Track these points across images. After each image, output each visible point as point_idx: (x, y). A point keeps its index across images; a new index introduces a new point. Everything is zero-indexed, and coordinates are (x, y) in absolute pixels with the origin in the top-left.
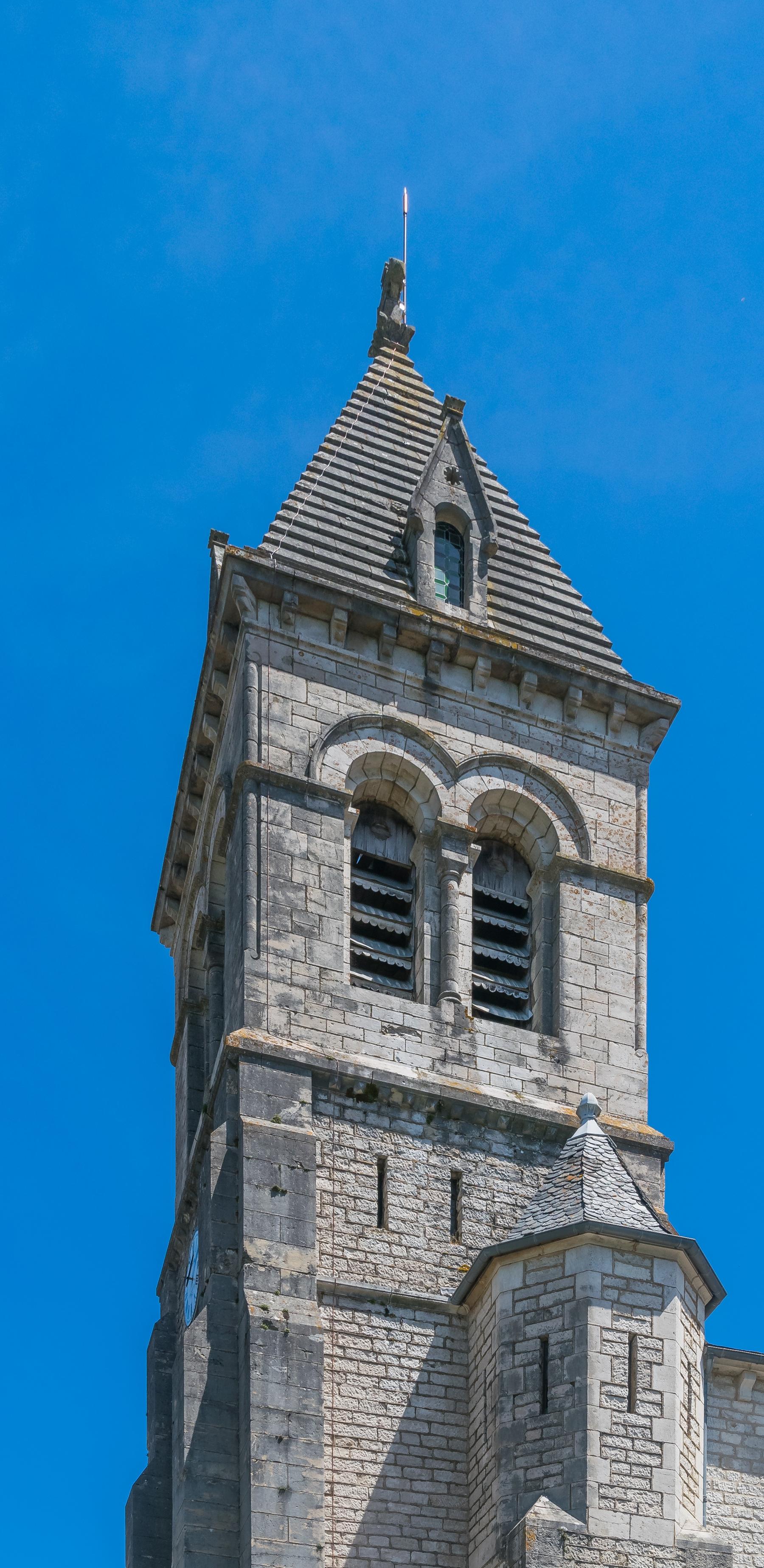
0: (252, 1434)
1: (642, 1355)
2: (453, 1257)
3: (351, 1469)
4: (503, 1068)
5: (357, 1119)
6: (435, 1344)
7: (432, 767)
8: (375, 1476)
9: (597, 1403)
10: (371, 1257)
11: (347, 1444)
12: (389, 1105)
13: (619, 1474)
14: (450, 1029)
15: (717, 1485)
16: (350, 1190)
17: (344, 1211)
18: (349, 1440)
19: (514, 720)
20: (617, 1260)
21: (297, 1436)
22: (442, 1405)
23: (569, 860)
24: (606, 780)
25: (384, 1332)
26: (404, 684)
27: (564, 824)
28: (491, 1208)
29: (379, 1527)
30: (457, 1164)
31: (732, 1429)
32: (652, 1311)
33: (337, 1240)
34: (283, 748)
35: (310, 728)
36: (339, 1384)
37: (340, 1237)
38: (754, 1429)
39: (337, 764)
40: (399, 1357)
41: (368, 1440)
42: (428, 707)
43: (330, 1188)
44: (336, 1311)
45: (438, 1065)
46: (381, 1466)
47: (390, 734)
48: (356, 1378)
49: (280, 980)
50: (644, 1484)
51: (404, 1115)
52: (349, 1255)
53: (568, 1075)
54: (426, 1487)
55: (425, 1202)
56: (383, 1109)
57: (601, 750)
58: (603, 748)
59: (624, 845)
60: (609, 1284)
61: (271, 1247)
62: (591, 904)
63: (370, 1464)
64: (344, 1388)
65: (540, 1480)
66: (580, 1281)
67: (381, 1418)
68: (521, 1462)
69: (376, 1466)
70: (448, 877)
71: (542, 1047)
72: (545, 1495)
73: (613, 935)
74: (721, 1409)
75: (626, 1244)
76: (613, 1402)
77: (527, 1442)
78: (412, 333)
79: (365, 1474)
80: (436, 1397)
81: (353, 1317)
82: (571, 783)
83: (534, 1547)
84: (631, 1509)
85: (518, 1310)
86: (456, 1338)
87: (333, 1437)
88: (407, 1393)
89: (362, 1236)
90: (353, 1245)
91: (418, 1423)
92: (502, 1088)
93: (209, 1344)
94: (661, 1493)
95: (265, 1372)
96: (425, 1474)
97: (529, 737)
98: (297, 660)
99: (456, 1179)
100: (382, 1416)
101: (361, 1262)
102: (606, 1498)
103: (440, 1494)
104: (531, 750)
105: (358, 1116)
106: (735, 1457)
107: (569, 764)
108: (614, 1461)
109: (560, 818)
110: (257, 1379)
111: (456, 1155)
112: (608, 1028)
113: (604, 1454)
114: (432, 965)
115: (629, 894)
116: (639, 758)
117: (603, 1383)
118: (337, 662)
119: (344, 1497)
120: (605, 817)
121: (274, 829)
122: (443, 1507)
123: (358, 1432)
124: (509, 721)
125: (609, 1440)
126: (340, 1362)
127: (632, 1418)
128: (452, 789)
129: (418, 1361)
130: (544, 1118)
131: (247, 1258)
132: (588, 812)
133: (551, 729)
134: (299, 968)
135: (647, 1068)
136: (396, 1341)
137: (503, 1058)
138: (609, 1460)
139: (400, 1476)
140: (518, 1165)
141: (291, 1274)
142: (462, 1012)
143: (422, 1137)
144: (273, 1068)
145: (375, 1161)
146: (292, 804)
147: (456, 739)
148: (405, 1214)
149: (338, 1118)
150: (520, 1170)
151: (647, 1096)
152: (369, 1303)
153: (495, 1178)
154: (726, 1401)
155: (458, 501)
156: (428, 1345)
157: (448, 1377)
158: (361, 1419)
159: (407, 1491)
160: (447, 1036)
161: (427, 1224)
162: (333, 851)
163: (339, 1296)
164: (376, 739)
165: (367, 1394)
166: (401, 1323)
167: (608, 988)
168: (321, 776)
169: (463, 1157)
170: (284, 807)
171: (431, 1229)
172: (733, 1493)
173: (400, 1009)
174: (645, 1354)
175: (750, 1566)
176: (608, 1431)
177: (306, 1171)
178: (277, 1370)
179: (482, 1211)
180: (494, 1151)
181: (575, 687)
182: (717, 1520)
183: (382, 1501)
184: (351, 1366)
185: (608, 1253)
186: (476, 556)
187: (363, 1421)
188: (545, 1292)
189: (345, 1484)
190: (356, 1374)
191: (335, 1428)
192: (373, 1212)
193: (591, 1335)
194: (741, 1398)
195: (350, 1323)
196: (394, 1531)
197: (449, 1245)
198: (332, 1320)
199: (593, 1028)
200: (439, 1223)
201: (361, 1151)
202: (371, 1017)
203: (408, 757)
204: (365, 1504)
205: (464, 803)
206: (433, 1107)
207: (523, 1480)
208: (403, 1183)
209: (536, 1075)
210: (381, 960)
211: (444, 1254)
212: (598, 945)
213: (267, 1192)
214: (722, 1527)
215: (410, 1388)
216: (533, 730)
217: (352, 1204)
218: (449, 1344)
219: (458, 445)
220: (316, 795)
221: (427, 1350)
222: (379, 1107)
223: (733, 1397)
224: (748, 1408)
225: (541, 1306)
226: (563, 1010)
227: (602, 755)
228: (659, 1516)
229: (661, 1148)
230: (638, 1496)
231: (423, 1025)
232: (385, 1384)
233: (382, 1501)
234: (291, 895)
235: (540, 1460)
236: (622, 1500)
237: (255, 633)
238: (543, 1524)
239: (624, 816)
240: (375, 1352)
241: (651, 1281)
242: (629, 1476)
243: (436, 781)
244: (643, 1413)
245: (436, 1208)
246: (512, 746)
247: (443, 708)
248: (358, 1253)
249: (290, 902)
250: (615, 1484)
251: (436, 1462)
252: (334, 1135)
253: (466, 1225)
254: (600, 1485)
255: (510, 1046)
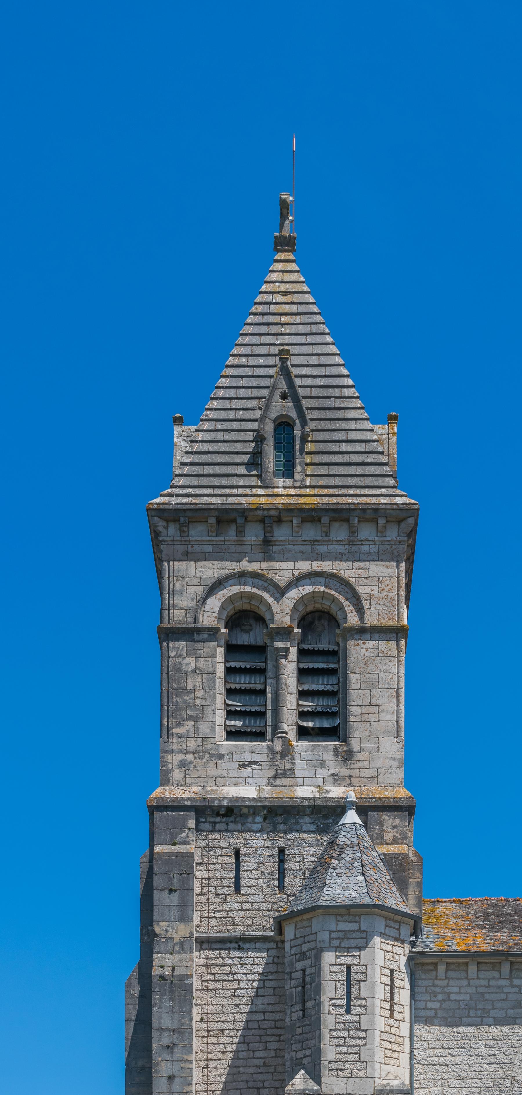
0: (153, 1046)
1: (354, 977)
2: (279, 903)
3: (219, 1050)
4: (311, 773)
5: (223, 829)
6: (268, 962)
7: (268, 592)
8: (232, 1052)
9: (327, 1011)
10: (231, 914)
11: (217, 1034)
12: (241, 816)
13: (340, 1054)
14: (279, 756)
15: (424, 1038)
16: (218, 874)
17: (214, 888)
18: (217, 1032)
19: (318, 545)
20: (339, 921)
21: (178, 1043)
22: (272, 1000)
23: (351, 627)
24: (377, 565)
25: (238, 959)
26: (252, 545)
27: (350, 603)
28: (302, 867)
29: (234, 1084)
30: (282, 843)
31: (435, 999)
32: (360, 948)
33: (211, 907)
34: (182, 609)
35: (197, 591)
36: (211, 998)
37: (213, 905)
38: (449, 997)
39: (213, 609)
40: (247, 974)
41: (228, 1030)
42: (266, 554)
43: (207, 876)
44: (210, 952)
45: (272, 781)
46: (235, 1045)
47: (243, 579)
48: (221, 992)
49: (180, 752)
50: (355, 1057)
51: (250, 819)
52: (218, 915)
53: (353, 766)
54: (262, 1054)
55: (262, 872)
57: (374, 546)
58: (375, 545)
59: (388, 604)
60: (334, 937)
62: (367, 650)
63: (229, 1045)
64: (214, 1000)
65: (302, 1059)
66: (319, 937)
67: (235, 1015)
68: (294, 1047)
69: (233, 1046)
70: (279, 657)
72: (303, 1069)
73: (381, 667)
74: (426, 987)
75: (343, 911)
76: (337, 1010)
77: (296, 1035)
78: (295, 238)
79: (226, 1052)
80: (268, 995)
81: (220, 954)
82: (354, 574)
84: (348, 1075)
85: (293, 953)
86: (280, 956)
87: (208, 1031)
88: (251, 996)
89: (225, 901)
91: (258, 1014)
92: (310, 786)
93: (139, 986)
94: (366, 1062)
95: (160, 1007)
96: (261, 1047)
97: (328, 553)
98: (189, 551)
99: (281, 851)
100: (237, 1013)
101: (225, 918)
102: (332, 1070)
103: (271, 1057)
104: (329, 561)
106: (436, 1017)
107: (353, 562)
108: (337, 1046)
109: (347, 599)
110: (156, 1012)
111: (281, 837)
113: (331, 1043)
114: (272, 712)
115: (391, 636)
116: (398, 544)
117: (331, 999)
118: (212, 545)
119: (214, 1068)
120: (376, 589)
121: (176, 660)
122: (272, 1066)
123: (223, 1026)
124: (316, 546)
125: (334, 1034)
126: (212, 983)
127: (348, 1017)
128: (280, 602)
129: (257, 975)
130: (332, 804)
131: (156, 935)
133: (342, 543)
134: (191, 742)
135: (403, 749)
136: (245, 964)
137: (311, 766)
138: (334, 1046)
139: (247, 1049)
140: (320, 835)
141: (180, 940)
142: (287, 743)
143: (260, 831)
144: (173, 811)
145: (233, 853)
146: (187, 641)
147: (283, 569)
148: (251, 882)
149: (212, 831)
150: (320, 838)
151: (403, 768)
152: (229, 943)
153: (305, 847)
154: (430, 981)
155: (287, 411)
156: (263, 963)
157: (275, 981)
158: (224, 1017)
159: (251, 1058)
160: (277, 761)
161: (264, 885)
162: (210, 663)
163: (211, 943)
164: (235, 585)
165: (228, 1001)
166: (247, 953)
167: (379, 702)
168: (203, 619)
169: (285, 837)
171: (266, 888)
172: (434, 1041)
173: (249, 751)
174: (355, 977)
175: (446, 1087)
176: (333, 1028)
177: (188, 874)
178: (167, 1005)
179: (297, 870)
180: (304, 829)
181: (353, 516)
182: (424, 1061)
183: (236, 1067)
184: (218, 985)
185: (333, 918)
186: (298, 443)
187: (225, 1018)
188: (304, 943)
189: (215, 1060)
190: (221, 989)
191: (209, 1025)
192: (232, 885)
193: (324, 971)
194: (438, 978)
195: (218, 958)
196: (243, 1085)
197: (277, 896)
198: (208, 958)
199: (368, 731)
200: (271, 883)
201: (225, 848)
202: (232, 761)
203: (254, 590)
204: (226, 1070)
205: (288, 608)
206: (265, 812)
207: (294, 1058)
208: (249, 862)
209: (332, 772)
210: (247, 710)
211: (274, 903)
212: (371, 676)
213: (166, 892)
214: (427, 1065)
215: (252, 993)
216: (330, 547)
218: (276, 960)
219: (287, 375)
220: (200, 632)
221: (262, 966)
222: (235, 818)
223: (434, 977)
224: (445, 983)
225: (302, 951)
226: (349, 724)
227: (374, 549)
228: (364, 1076)
229: (407, 805)
230: (352, 1065)
231: (263, 758)
232: (239, 993)
233: (236, 1067)
234: (186, 698)
235: (302, 1047)
236: (342, 1070)
237: (166, 543)
238: (295, 1091)
239: (388, 585)
240: (232, 974)
241: (359, 930)
242: (346, 1053)
243: (270, 600)
244: (355, 1013)
245: (269, 874)
246: (317, 562)
247: (275, 552)
248: (223, 913)
249: (185, 702)
250: (338, 1060)
251: (268, 1037)
252: (209, 842)
253: (287, 881)
254: (329, 1062)
255: (315, 757)
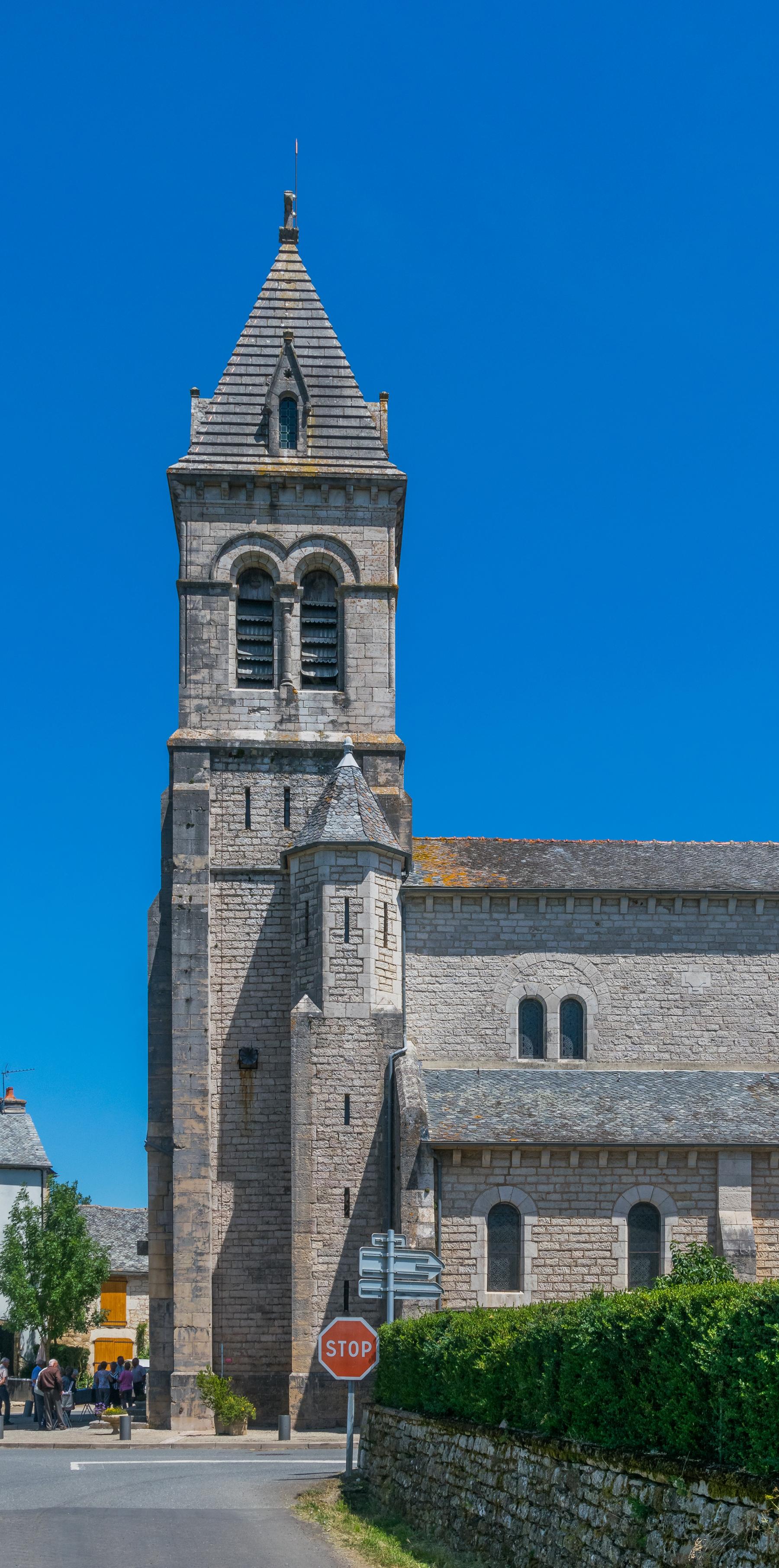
1: (352, 909)
7: (274, 552)
10: (242, 848)
12: (251, 757)
14: (284, 703)
30: (287, 783)
31: (423, 930)
32: (357, 882)
33: (224, 842)
43: (220, 812)
49: (197, 697)
50: (353, 983)
51: (259, 761)
52: (230, 849)
53: (350, 714)
56: (248, 760)
61: (186, 858)
62: (362, 607)
66: (320, 871)
71: (335, 700)
74: (416, 919)
83: (295, 1028)
89: (237, 836)
90: (232, 843)
95: (179, 934)
96: (270, 972)
99: (287, 790)
105: (235, 767)
106: (424, 947)
109: (344, 560)
112: (372, 679)
117: (331, 929)
120: (370, 552)
121: (193, 612)
123: (235, 953)
125: (335, 961)
127: (346, 946)
131: (175, 867)
132: (358, 552)
143: (268, 772)
149: (225, 771)
158: (236, 944)
167: (373, 655)
170: (198, 598)
184: (231, 914)
185: (333, 854)
196: (253, 1008)
198: (221, 889)
203: (262, 550)
204: (239, 994)
209: (331, 718)
213: (184, 827)
217: (232, 819)
224: (431, 916)
231: (270, 704)
232: (249, 921)
234: (202, 647)
236: (341, 995)
241: (356, 865)
249: (201, 651)
253: (292, 818)
254: (330, 988)
